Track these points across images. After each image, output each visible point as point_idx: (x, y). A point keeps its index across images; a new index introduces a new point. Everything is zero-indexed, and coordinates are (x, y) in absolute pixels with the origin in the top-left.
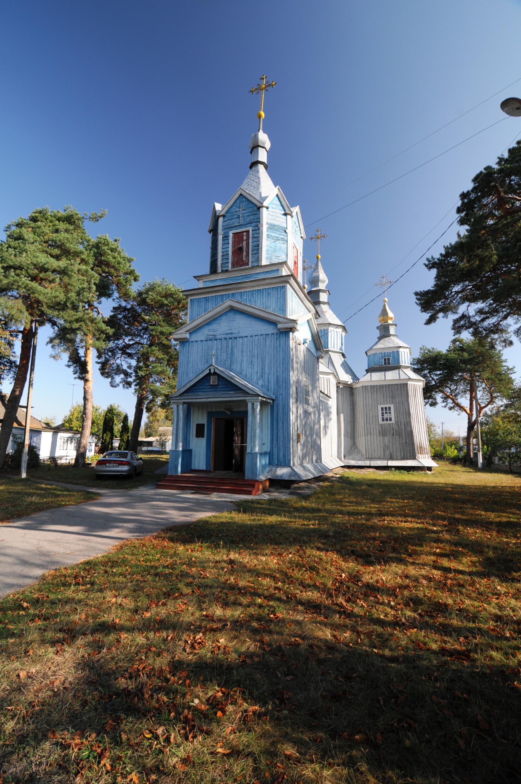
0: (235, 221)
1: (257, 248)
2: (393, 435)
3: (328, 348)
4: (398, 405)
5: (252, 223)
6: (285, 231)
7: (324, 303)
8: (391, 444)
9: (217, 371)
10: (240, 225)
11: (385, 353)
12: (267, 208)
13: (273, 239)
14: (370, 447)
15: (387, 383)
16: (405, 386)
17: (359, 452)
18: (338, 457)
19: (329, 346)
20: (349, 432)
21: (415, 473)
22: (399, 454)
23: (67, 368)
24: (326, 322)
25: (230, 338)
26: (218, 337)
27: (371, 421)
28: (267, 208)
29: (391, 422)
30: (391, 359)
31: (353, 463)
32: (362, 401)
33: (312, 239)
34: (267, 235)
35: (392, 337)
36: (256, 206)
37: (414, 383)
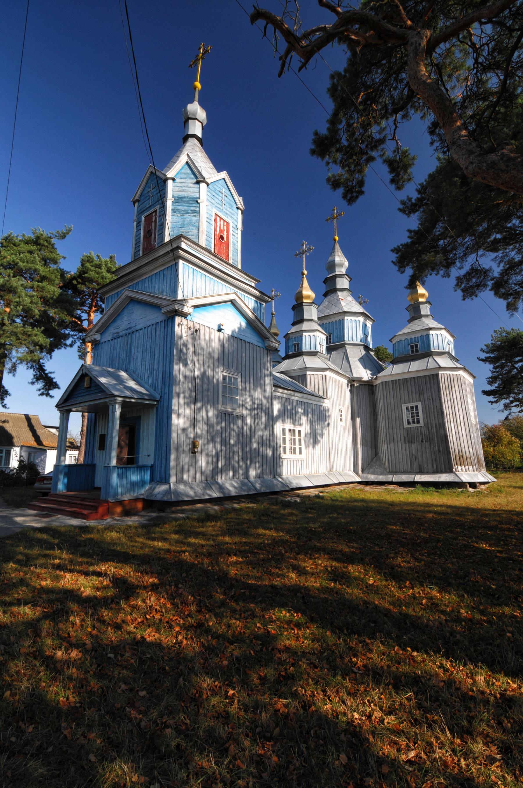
2: (422, 442)
3: (344, 340)
4: (427, 403)
6: (197, 201)
7: (342, 290)
8: (419, 454)
10: (151, 206)
11: (411, 339)
12: (173, 179)
13: (180, 213)
14: (393, 457)
15: (412, 376)
16: (435, 377)
17: (381, 464)
18: (354, 471)
19: (346, 338)
20: (369, 439)
21: (445, 491)
22: (430, 466)
23: (30, 385)
24: (340, 311)
25: (131, 332)
26: (121, 334)
27: (394, 425)
28: (173, 179)
29: (419, 425)
30: (419, 345)
31: (372, 478)
32: (382, 401)
33: (327, 220)
34: (172, 209)
35: (423, 319)
37: (448, 372)
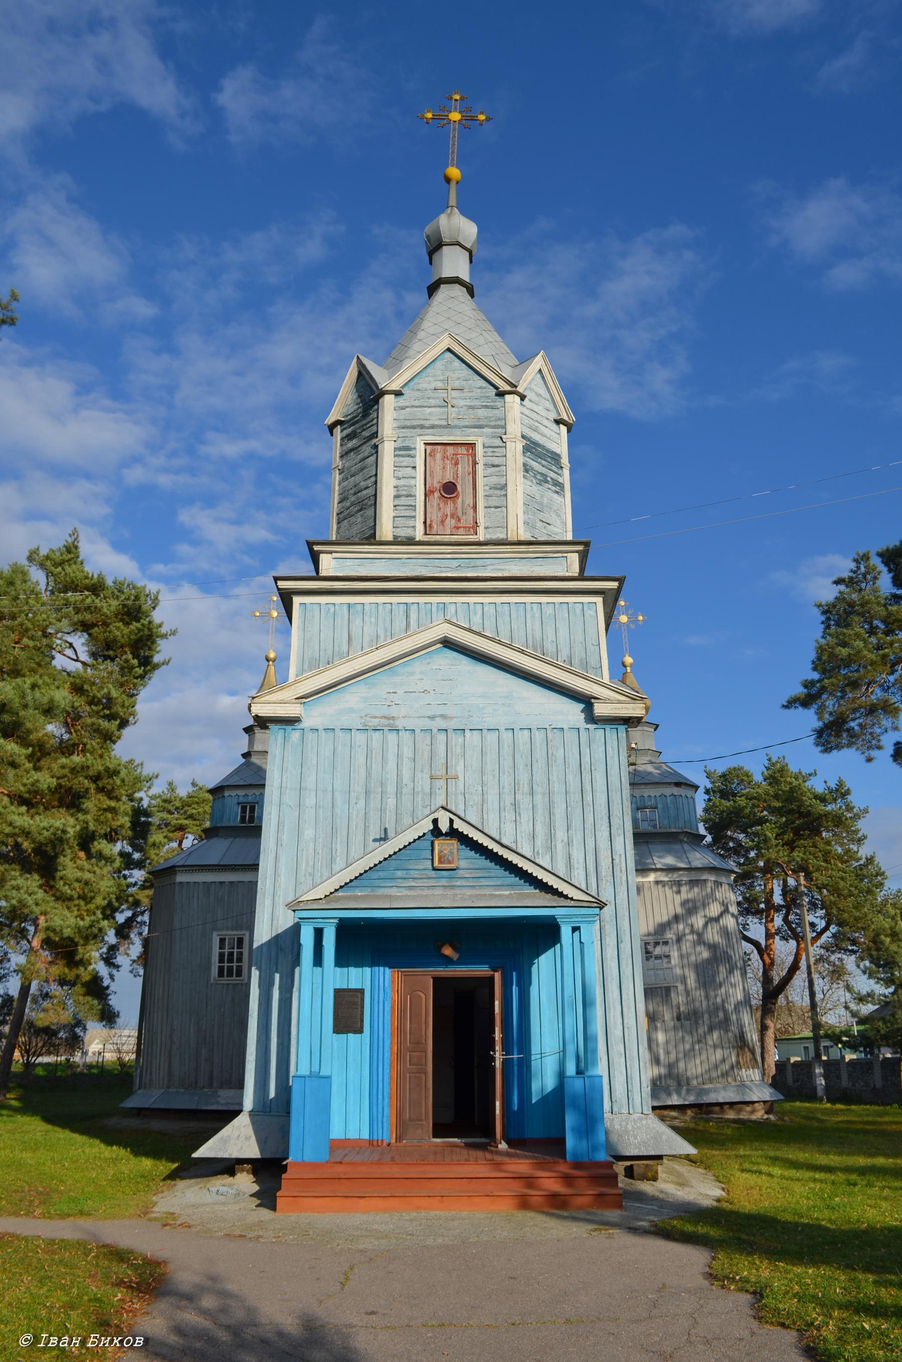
0: (430, 414)
1: (498, 492)
5: (481, 427)
9: (458, 825)
12: (523, 397)
26: (400, 724)
36: (496, 388)
